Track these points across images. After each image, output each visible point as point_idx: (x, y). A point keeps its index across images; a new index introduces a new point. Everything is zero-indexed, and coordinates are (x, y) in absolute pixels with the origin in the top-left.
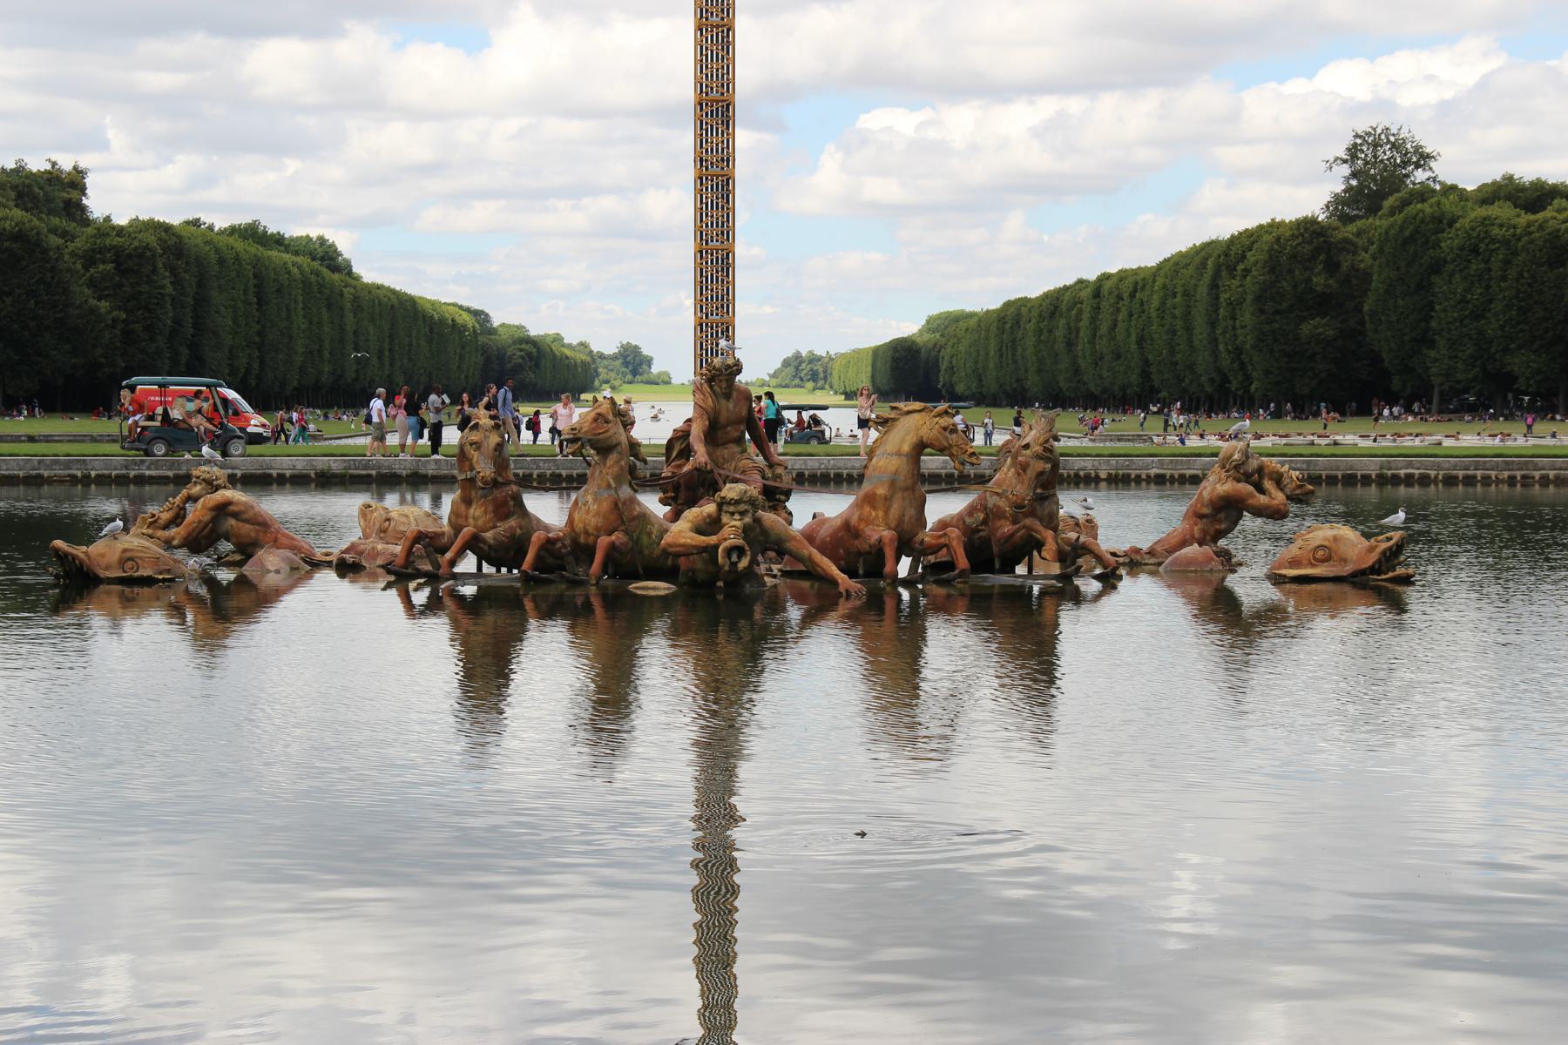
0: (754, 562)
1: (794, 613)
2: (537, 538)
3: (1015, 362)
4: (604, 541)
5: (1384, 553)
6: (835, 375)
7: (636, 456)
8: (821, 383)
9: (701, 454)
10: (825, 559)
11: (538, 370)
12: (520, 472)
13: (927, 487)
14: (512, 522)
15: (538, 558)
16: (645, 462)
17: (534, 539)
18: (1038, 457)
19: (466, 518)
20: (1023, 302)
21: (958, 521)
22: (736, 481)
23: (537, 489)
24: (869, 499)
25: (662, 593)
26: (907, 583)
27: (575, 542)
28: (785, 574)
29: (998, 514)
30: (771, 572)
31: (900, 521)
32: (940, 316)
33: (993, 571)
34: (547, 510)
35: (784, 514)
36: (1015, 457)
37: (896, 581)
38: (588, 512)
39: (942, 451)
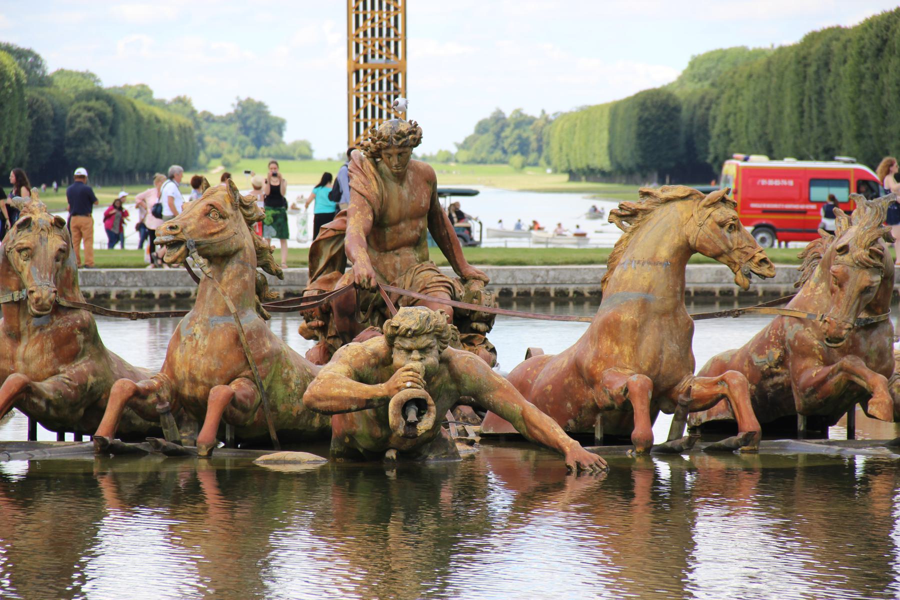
0: (441, 422)
1: (500, 500)
2: (118, 391)
3: (823, 123)
4: (218, 394)
6: (555, 144)
7: (266, 267)
8: (533, 157)
9: (361, 264)
10: (546, 418)
12: (92, 291)
13: (692, 310)
14: (82, 366)
15: (122, 418)
16: (280, 275)
17: (115, 389)
18: (863, 265)
19: (13, 359)
20: (836, 33)
21: (742, 360)
22: (413, 303)
23: (117, 315)
24: (610, 329)
25: (310, 467)
26: (666, 452)
27: (176, 394)
28: (487, 439)
29: (804, 351)
30: (463, 433)
31: (656, 361)
32: (721, 56)
33: (793, 434)
34: (134, 347)
35: (484, 351)
36: (827, 266)
37: (649, 449)
38: (195, 349)
39: (717, 257)
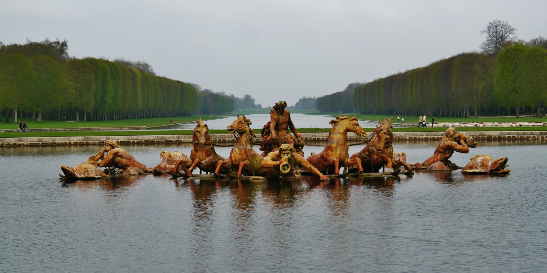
0: (291, 170)
2: (220, 162)
4: (242, 164)
5: (500, 164)
9: (273, 133)
11: (219, 104)
14: (211, 157)
15: (220, 169)
18: (385, 133)
21: (359, 155)
22: (285, 143)
26: (343, 176)
31: (340, 155)
34: (224, 153)
